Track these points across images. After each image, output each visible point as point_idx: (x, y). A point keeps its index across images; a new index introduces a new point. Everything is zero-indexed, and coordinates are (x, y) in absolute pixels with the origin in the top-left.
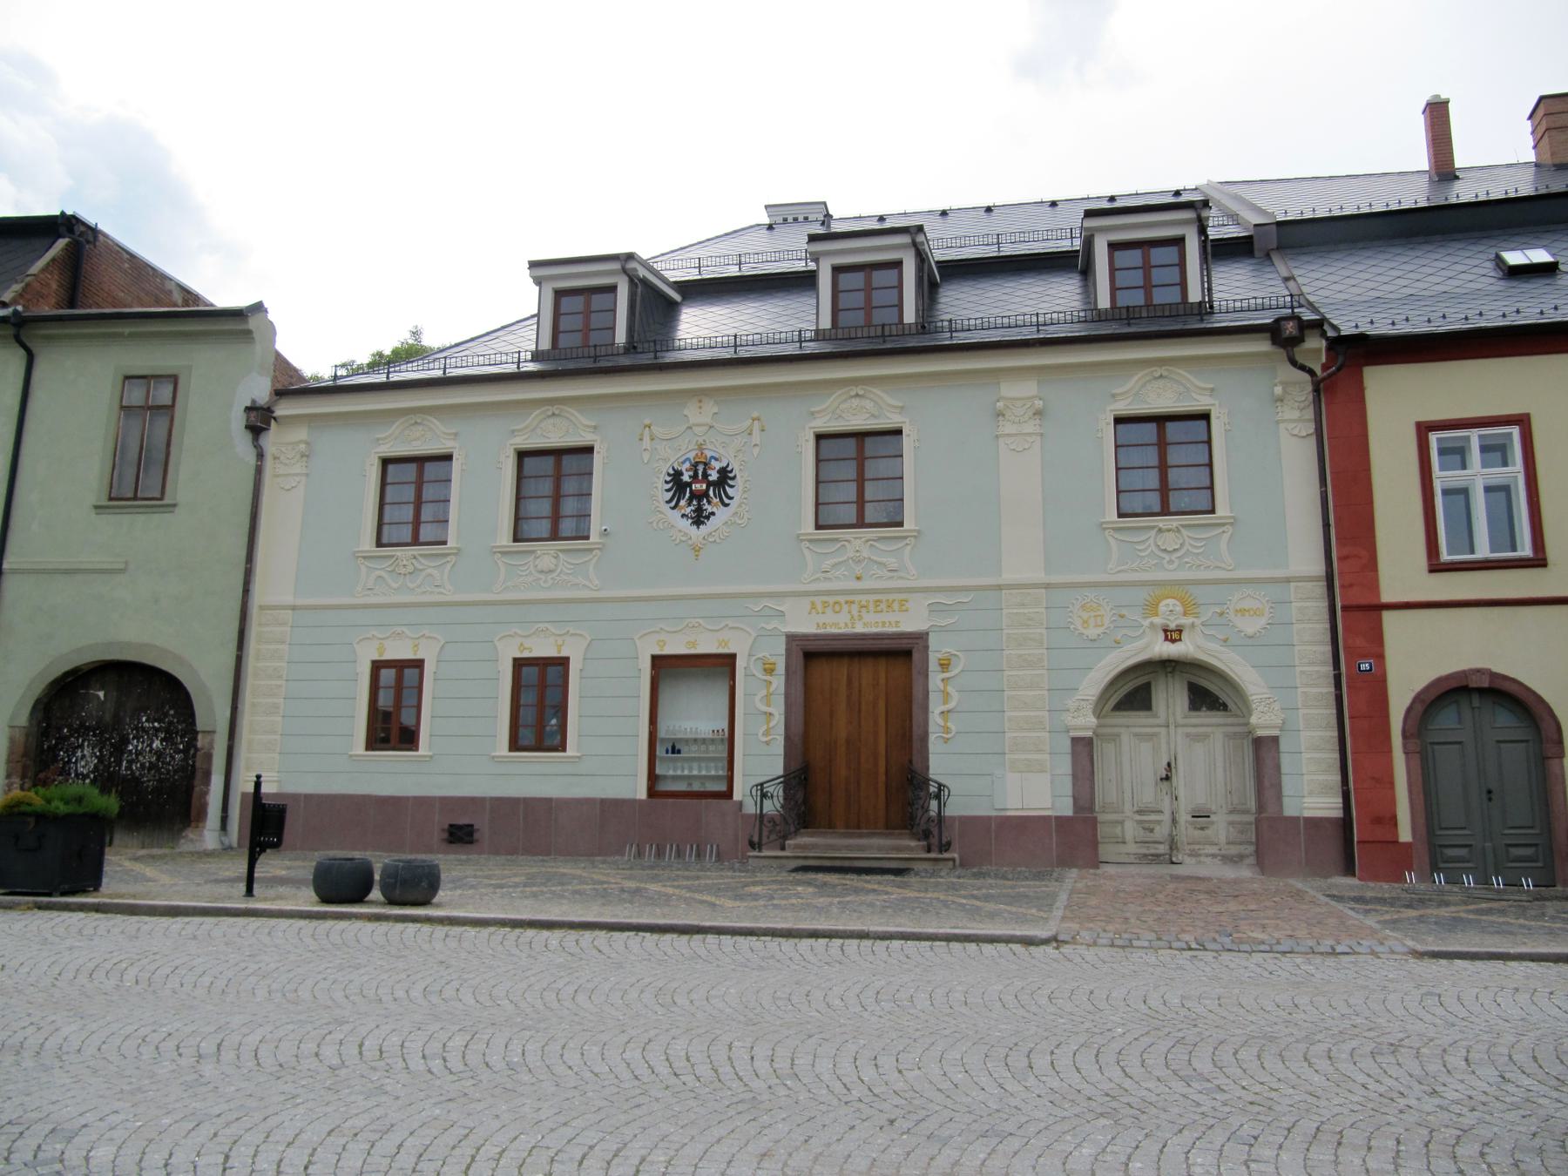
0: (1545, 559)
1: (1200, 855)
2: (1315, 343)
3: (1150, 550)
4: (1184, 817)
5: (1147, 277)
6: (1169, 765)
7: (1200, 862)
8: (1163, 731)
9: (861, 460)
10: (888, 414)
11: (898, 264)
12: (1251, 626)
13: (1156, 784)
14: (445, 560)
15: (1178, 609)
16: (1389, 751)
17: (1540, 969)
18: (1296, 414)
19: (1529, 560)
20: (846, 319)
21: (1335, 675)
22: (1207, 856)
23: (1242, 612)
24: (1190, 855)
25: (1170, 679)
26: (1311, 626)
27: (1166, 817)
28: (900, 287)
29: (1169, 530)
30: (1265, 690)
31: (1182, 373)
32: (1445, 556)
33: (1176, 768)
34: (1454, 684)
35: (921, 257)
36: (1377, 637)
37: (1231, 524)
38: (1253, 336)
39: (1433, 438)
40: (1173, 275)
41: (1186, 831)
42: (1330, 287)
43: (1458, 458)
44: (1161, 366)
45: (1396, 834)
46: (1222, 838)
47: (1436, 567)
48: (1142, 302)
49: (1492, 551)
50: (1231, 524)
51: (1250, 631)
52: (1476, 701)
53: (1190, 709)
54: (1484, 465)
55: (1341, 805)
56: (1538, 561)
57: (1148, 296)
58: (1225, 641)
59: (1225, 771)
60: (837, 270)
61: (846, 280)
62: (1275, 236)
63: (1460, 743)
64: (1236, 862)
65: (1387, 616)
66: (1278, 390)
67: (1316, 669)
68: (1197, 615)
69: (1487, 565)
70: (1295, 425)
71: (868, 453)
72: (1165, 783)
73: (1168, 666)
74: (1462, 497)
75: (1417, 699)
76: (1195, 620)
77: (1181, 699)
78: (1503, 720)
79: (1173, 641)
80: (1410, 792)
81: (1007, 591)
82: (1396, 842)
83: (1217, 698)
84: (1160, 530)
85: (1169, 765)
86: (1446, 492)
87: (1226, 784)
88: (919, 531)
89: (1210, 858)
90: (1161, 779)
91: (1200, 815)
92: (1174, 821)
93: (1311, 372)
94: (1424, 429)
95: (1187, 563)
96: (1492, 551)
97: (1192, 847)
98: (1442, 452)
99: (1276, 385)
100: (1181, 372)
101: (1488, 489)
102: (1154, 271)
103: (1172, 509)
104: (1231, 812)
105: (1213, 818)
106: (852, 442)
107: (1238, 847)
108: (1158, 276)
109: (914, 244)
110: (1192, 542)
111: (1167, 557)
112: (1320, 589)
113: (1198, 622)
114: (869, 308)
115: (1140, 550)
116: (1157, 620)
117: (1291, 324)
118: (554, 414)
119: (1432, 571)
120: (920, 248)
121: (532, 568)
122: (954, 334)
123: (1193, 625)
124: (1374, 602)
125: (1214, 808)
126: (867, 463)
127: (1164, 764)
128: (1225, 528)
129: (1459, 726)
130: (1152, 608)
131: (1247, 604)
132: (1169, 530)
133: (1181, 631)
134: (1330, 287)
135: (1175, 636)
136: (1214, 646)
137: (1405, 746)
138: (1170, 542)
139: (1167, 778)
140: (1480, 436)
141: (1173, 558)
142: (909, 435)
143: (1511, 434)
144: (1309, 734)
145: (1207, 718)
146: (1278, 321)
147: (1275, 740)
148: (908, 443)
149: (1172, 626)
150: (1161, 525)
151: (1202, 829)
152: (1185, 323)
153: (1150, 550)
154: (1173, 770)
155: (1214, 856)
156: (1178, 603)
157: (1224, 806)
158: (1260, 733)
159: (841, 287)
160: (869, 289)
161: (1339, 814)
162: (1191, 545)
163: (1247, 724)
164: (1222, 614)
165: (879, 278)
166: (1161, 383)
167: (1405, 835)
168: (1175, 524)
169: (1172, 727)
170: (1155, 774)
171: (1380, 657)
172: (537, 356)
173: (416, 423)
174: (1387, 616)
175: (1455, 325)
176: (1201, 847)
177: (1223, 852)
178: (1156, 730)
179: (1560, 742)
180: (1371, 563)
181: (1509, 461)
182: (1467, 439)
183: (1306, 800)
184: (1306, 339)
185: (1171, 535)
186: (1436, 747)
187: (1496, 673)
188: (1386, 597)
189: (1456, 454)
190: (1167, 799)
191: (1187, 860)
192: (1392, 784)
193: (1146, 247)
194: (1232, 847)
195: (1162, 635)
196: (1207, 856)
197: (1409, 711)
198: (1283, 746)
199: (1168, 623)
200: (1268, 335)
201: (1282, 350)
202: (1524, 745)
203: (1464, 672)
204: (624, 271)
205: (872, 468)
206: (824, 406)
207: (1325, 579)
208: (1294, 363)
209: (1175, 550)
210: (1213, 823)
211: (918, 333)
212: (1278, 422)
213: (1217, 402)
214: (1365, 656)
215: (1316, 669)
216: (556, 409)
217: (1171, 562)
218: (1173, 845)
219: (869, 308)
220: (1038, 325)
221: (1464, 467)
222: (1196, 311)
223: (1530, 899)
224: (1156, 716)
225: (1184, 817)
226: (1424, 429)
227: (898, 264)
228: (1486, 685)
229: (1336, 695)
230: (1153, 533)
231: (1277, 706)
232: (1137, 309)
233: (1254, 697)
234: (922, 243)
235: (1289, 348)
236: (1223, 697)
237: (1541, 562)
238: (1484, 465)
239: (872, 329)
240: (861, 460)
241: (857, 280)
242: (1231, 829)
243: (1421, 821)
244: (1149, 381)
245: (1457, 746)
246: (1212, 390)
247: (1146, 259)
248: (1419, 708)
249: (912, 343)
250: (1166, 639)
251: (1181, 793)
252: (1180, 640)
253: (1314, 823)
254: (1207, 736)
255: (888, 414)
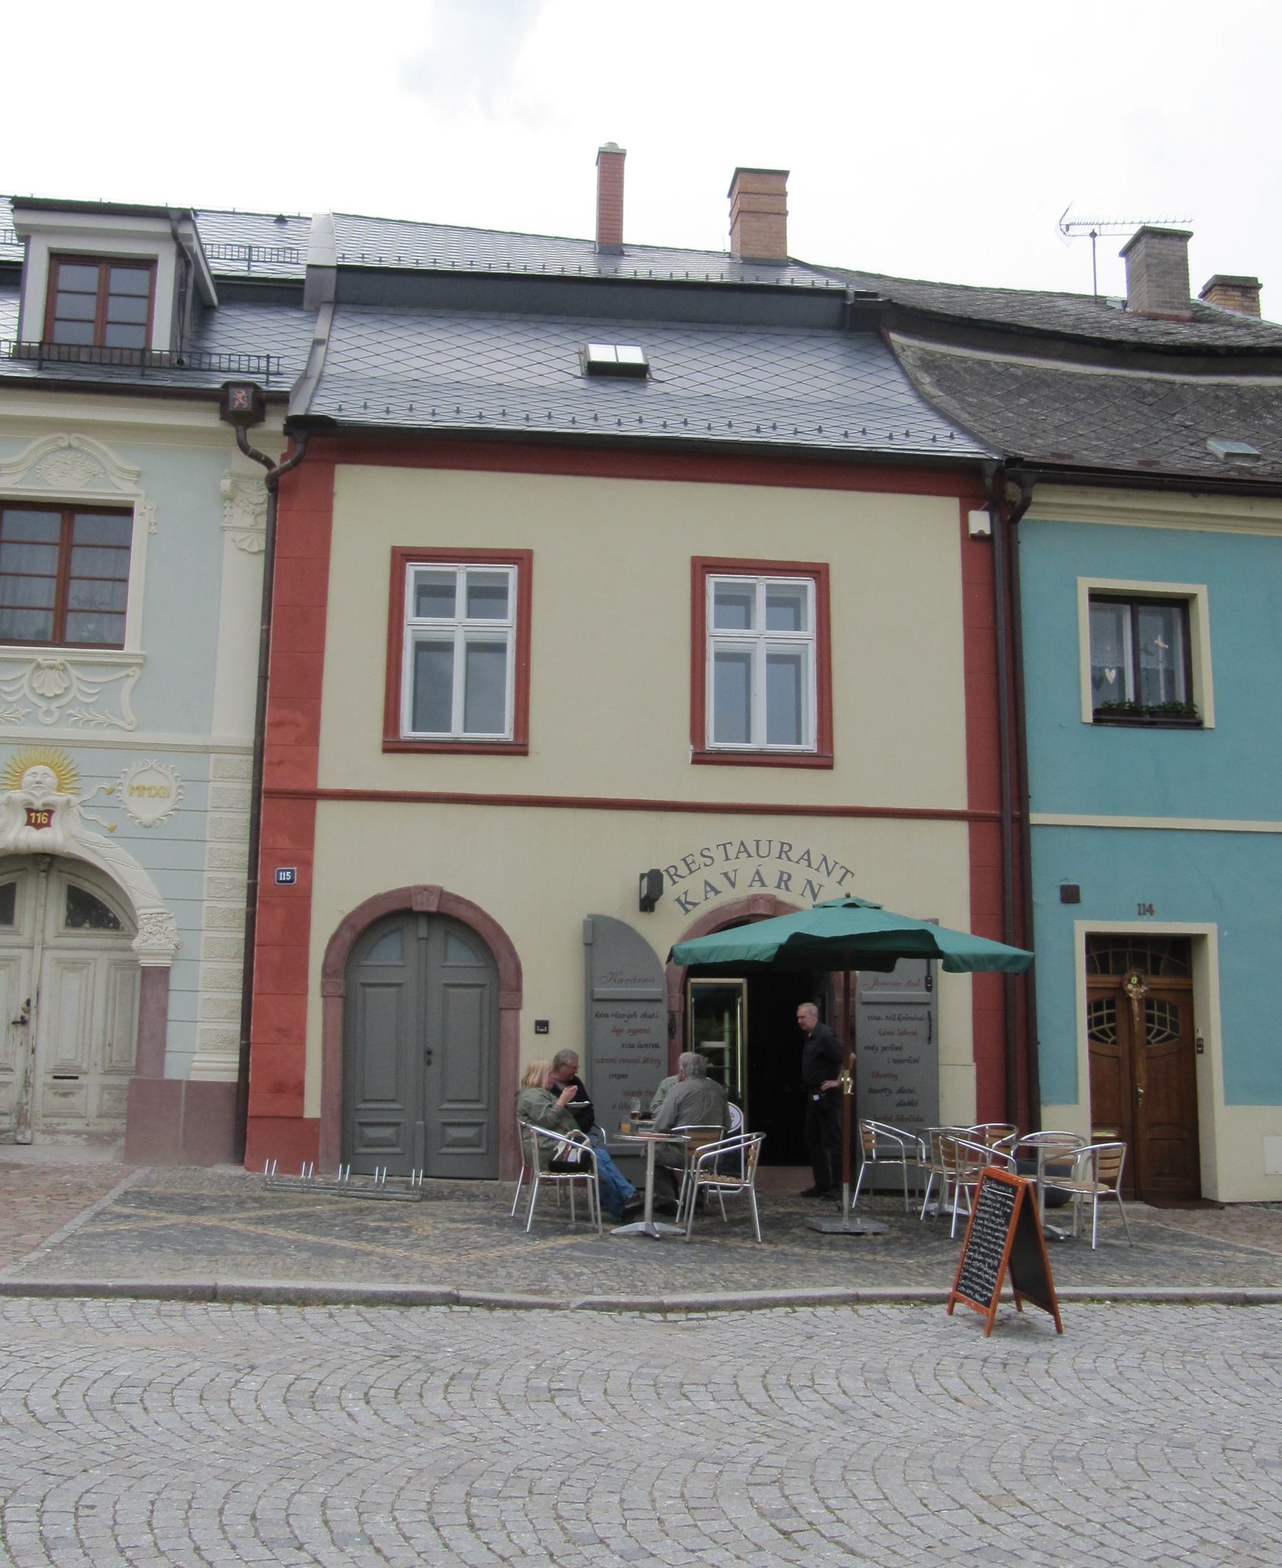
0: (526, 745)
1: (59, 1132)
2: (275, 423)
3: (20, 695)
4: (42, 1078)
5: (102, 307)
6: (28, 1002)
7: (56, 1143)
8: (25, 954)
9: (66, 547)
10: (118, 482)
11: (148, 264)
12: (148, 810)
13: (8, 1029)
14: (123, 673)
15: (48, 780)
16: (305, 993)
17: (1264, 1311)
18: (248, 521)
19: (810, 755)
20: (64, 334)
21: (249, 885)
22: (68, 1133)
23: (140, 790)
24: (43, 1132)
25: (47, 878)
26: (231, 816)
27: (17, 1078)
28: (150, 297)
29: (51, 668)
30: (158, 903)
31: (100, 446)
32: (712, 743)
33: (37, 1007)
34: (395, 906)
35: (187, 259)
36: (305, 835)
37: (140, 665)
38: (194, 404)
39: (712, 581)
40: (65, 306)
41: (44, 1097)
42: (709, 372)
43: (790, 612)
44: (68, 432)
45: (301, 1107)
46: (92, 1110)
47: (393, 746)
48: (89, 340)
49: (769, 741)
50: (140, 665)
51: (147, 817)
52: (423, 930)
53: (67, 924)
54: (771, 625)
55: (237, 1065)
56: (822, 761)
57: (100, 333)
58: (112, 829)
59: (106, 1013)
60: (58, 258)
61: (72, 276)
62: (334, 281)
63: (398, 985)
64: (108, 1143)
65: (323, 808)
66: (226, 484)
67: (229, 875)
68: (77, 791)
69: (456, 747)
70: (244, 535)
71: (79, 537)
72: (21, 1029)
73: (46, 862)
74: (792, 667)
75: (346, 923)
76: (71, 797)
77: (56, 909)
78: (460, 955)
79: (38, 826)
80: (324, 1050)
81: (218, 756)
82: (300, 1118)
83: (107, 910)
84: (39, 667)
85: (28, 1002)
86: (720, 657)
87: (105, 1034)
88: (145, 658)
89: (71, 1137)
90: (14, 1023)
91: (65, 1076)
92: (27, 1084)
93: (268, 463)
94: (401, 557)
95: (71, 715)
96: (769, 741)
97: (49, 1120)
98: (720, 600)
99: (225, 478)
100: (97, 443)
101: (772, 659)
102: (112, 300)
103: (420, 653)
104: (108, 1072)
105: (83, 1080)
106: (55, 519)
107: (113, 1121)
108: (87, 307)
109: (175, 236)
110: (83, 688)
111: (43, 705)
112: (245, 764)
113: (75, 800)
114: (101, 322)
115: (5, 693)
116: (18, 795)
117: (243, 393)
118: (70, 447)
119: (387, 749)
120: (184, 244)
121: (26, 690)
122: (272, 378)
123: (68, 804)
124: (302, 785)
125: (85, 1066)
126: (77, 554)
127: (22, 1003)
128: (129, 671)
129: (401, 963)
130: (15, 777)
131: (148, 780)
132: (51, 668)
133: (50, 812)
134: (709, 372)
135: (42, 819)
136: (95, 836)
137: (323, 985)
138: (52, 683)
139: (23, 1022)
140: (768, 586)
141: (53, 709)
142: (142, 514)
143: (805, 587)
144: (210, 965)
145: (91, 938)
146: (227, 385)
147: (164, 972)
148: (140, 523)
149: (38, 805)
150: (40, 659)
151: (66, 1095)
152: (150, 377)
153: (20, 695)
154: (33, 1011)
155: (77, 1133)
156: (51, 772)
157: (99, 1062)
158: (146, 962)
159: (63, 284)
160: (103, 295)
161: (233, 1077)
162: (79, 690)
163: (130, 949)
164: (111, 792)
165: (121, 279)
166: (70, 455)
167: (312, 1108)
168: (60, 659)
169: (38, 950)
170: (8, 1015)
171: (306, 864)
172: (20, 353)
173: (70, 447)
174: (323, 808)
175: (743, 434)
176: (62, 1120)
177: (91, 1128)
178: (15, 952)
179: (518, 989)
180: (311, 736)
181: (802, 626)
182: (753, 587)
183: (196, 1058)
184: (267, 418)
185: (52, 673)
186: (368, 990)
187: (449, 894)
188: (324, 783)
189: (739, 603)
190: (21, 1051)
191: (39, 1138)
192: (302, 1038)
193: (104, 265)
194: (104, 1121)
195: (23, 817)
196: (68, 1133)
197: (335, 938)
198: (175, 980)
199: (34, 800)
200: (217, 405)
201: (233, 429)
202: (478, 990)
203: (408, 889)
204: (175, 236)
205: (81, 563)
206: (17, 458)
207: (252, 752)
208: (244, 448)
209: (56, 696)
210: (80, 1087)
211: (172, 368)
212: (223, 529)
213: (143, 493)
214: (285, 861)
215: (229, 875)
216: (71, 439)
217: (48, 712)
218: (23, 1119)
219: (101, 322)
220: (268, 373)
221: (748, 625)
222: (136, 361)
223: (417, 1197)
224: (17, 933)
225: (42, 1078)
226: (401, 557)
227: (148, 264)
228: (433, 908)
229: (248, 913)
230: (29, 669)
231: (172, 925)
232: (74, 350)
233: (142, 911)
234: (189, 237)
235: (241, 428)
236: (115, 910)
237: (521, 749)
238: (771, 625)
239: (106, 352)
240: (66, 547)
241: (87, 277)
242: (106, 1096)
243: (336, 1087)
244: (53, 452)
245: (394, 990)
246: (139, 474)
247: (104, 281)
248: (348, 936)
249: (168, 382)
250: (29, 823)
251: (43, 1045)
252: (48, 825)
253: (200, 1090)
254: (86, 963)
255: (118, 482)
